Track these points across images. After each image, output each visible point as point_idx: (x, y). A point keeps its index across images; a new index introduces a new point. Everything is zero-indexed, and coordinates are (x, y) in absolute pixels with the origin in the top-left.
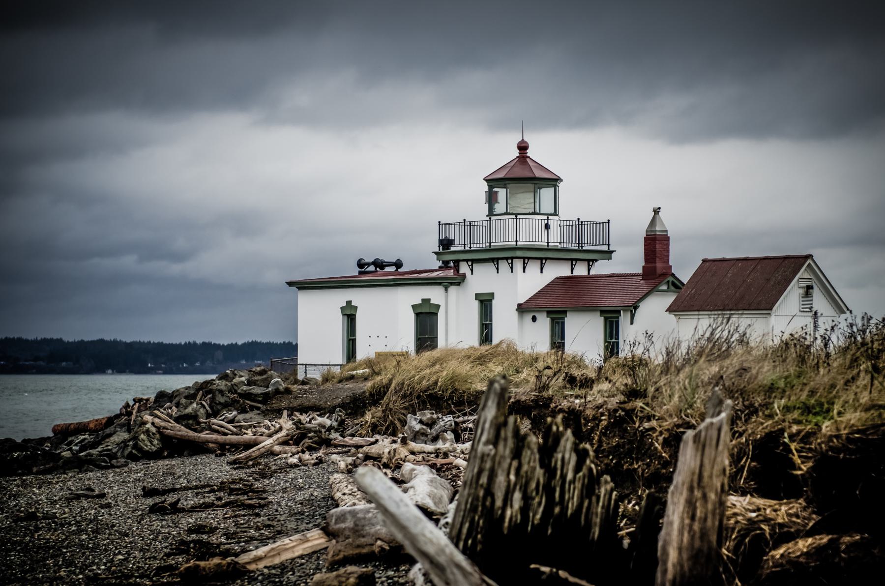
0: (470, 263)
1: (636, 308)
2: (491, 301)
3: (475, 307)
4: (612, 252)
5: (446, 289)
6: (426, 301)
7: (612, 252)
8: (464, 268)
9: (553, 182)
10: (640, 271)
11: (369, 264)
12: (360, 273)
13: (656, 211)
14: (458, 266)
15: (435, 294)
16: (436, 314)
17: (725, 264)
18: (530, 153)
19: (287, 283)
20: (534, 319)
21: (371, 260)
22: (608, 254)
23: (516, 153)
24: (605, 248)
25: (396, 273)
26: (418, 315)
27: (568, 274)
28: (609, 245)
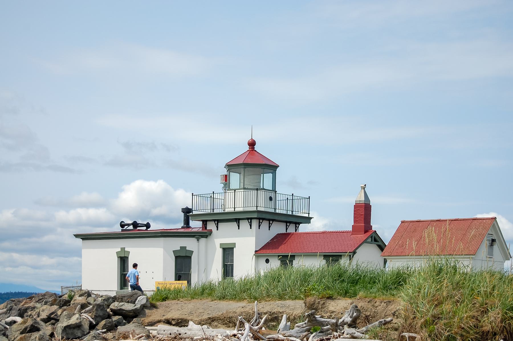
0: (216, 222)
1: (354, 253)
2: (233, 248)
3: (219, 253)
4: (311, 218)
5: (198, 240)
6: (183, 248)
7: (311, 218)
8: (211, 226)
9: (272, 168)
10: (351, 229)
11: (129, 225)
12: (122, 230)
13: (77, 236)
14: (206, 224)
15: (190, 244)
16: (190, 257)
17: (421, 224)
18: (256, 148)
19: (74, 235)
20: (267, 261)
21: (130, 222)
22: (308, 220)
23: (247, 148)
24: (307, 215)
25: (146, 230)
26: (176, 257)
27: (284, 231)
28: (309, 214)
